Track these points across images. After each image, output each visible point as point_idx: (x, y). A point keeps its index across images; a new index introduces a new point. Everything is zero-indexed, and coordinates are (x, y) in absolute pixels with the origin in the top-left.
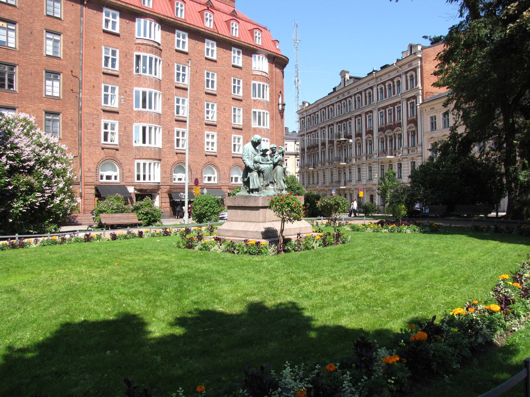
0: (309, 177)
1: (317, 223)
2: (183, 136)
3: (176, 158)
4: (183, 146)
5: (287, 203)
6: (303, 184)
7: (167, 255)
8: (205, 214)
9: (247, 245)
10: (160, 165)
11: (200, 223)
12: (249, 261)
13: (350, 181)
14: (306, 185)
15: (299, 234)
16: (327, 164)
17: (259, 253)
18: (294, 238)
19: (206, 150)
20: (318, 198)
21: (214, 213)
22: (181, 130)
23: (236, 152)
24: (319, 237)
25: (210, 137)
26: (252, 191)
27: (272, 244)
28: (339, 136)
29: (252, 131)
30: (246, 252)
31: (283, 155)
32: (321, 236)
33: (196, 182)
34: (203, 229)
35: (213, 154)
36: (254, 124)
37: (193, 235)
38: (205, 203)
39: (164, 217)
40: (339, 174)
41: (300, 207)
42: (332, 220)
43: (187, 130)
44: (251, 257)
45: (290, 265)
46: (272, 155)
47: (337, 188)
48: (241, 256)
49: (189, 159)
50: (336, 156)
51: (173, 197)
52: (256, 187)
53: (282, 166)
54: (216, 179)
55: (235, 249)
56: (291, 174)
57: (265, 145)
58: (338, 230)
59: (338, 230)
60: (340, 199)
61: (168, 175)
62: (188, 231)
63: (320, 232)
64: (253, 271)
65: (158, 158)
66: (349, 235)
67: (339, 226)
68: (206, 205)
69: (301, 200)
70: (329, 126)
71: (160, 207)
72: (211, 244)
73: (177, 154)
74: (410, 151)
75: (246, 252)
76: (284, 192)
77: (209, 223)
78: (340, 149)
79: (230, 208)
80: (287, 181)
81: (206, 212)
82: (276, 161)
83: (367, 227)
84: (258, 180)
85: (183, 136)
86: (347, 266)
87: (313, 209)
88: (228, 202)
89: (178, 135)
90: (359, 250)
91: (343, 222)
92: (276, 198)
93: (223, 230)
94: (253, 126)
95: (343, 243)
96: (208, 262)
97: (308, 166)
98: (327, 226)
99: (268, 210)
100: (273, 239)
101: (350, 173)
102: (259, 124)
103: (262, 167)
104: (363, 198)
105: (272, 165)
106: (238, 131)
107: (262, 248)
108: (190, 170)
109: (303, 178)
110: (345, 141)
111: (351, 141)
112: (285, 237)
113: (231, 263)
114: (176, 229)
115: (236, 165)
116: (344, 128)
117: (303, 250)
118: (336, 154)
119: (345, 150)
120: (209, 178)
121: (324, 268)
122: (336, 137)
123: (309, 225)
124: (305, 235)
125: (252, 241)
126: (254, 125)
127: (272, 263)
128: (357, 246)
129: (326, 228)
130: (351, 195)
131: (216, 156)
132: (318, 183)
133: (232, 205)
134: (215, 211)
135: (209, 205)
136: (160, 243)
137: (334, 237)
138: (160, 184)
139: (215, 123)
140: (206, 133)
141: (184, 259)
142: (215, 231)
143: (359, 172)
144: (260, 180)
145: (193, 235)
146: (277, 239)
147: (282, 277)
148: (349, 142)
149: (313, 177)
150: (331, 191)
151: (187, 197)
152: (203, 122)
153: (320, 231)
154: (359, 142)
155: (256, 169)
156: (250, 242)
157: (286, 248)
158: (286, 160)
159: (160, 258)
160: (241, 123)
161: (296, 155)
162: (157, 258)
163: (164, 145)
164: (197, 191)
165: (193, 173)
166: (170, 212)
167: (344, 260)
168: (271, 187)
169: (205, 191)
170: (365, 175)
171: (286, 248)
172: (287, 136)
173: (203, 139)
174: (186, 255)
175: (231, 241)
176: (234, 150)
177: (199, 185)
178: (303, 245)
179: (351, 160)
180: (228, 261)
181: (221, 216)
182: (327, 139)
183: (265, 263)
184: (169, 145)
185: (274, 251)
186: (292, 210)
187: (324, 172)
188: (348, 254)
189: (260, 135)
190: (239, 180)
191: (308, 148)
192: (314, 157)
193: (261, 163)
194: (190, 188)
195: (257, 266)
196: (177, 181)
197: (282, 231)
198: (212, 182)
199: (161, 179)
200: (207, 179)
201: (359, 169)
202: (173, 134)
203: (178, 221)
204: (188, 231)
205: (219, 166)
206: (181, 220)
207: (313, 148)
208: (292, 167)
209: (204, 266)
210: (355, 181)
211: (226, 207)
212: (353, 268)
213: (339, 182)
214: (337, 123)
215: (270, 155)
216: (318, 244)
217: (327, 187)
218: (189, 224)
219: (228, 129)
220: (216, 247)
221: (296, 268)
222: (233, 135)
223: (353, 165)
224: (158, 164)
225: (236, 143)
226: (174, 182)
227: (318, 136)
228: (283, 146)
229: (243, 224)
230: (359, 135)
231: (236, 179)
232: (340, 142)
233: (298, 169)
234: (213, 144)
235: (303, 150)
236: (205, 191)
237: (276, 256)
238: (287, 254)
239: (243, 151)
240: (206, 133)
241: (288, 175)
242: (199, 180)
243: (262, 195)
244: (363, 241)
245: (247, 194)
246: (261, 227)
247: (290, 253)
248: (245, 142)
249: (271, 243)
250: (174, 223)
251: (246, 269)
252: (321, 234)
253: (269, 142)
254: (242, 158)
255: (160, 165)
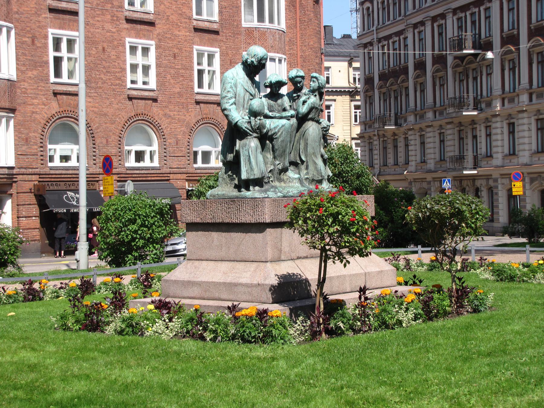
0: (385, 148)
1: (408, 261)
2: (70, 49)
3: (54, 107)
4: (71, 74)
5: (331, 215)
6: (372, 166)
7: (33, 349)
8: (129, 242)
9: (236, 318)
10: (12, 123)
11: (119, 265)
12: (242, 358)
13: (489, 156)
14: (377, 166)
15: (363, 290)
16: (430, 115)
17: (267, 337)
18: (351, 299)
19: (129, 85)
20: (409, 198)
21: (152, 241)
22: (65, 34)
23: (205, 89)
24: (413, 297)
25: (139, 52)
26: (246, 184)
27: (297, 316)
28: (460, 44)
29: (243, 38)
30: (233, 338)
31: (321, 95)
32: (418, 295)
33: (108, 165)
34: (127, 280)
35: (146, 94)
36: (249, 17)
37: (101, 296)
38: (129, 215)
39: (27, 254)
40: (461, 139)
41: (365, 222)
42: (444, 253)
43: (78, 35)
44: (245, 348)
45: (343, 368)
46: (294, 96)
47: (455, 174)
48: (222, 345)
49: (87, 108)
50: (451, 95)
51: (47, 202)
52: (256, 174)
53: (318, 122)
54: (156, 158)
55: (205, 329)
56: (340, 142)
57: (276, 71)
58: (460, 279)
59: (460, 279)
60: (465, 203)
61: (35, 149)
62: (87, 287)
63: (414, 284)
64: (252, 383)
65: (7, 105)
66: (490, 291)
67: (465, 267)
68: (133, 221)
69: (367, 205)
70: (434, 19)
71: (17, 229)
72: (147, 319)
73: (55, 94)
74: (534, 97)
75: (233, 338)
76: (326, 186)
77: (139, 265)
78: (462, 76)
79: (192, 227)
80: (331, 159)
81: (133, 239)
82: (304, 109)
83: (534, 272)
84: (260, 158)
85: (70, 49)
86: (486, 369)
87: (396, 231)
88: (187, 212)
89: (57, 48)
90: (517, 328)
91: (473, 258)
92: (305, 203)
93: (176, 282)
94: (244, 24)
95: (476, 310)
96: (139, 365)
97: (383, 121)
98: (431, 268)
99: (286, 232)
100: (298, 304)
101: (489, 135)
102: (261, 18)
103: (269, 124)
104: (522, 198)
105: (294, 121)
106: (207, 36)
107: (272, 326)
108: (91, 134)
109: (371, 150)
110: (475, 55)
111: (490, 55)
112: (331, 298)
113: (196, 365)
114: (58, 283)
115: (206, 122)
116: (473, 23)
117: (376, 329)
118: (451, 89)
119: (475, 79)
120: (140, 156)
121: (430, 375)
122: (453, 48)
123: (388, 267)
124: (377, 292)
125: (249, 309)
126: (249, 20)
127: (297, 363)
128: (513, 319)
129: (430, 274)
130: (491, 191)
131: (155, 100)
132: (407, 163)
133: (198, 220)
134: (156, 236)
135: (139, 221)
136: (16, 319)
137: (451, 297)
138: (15, 171)
139: (151, 17)
140: (129, 41)
141: (78, 358)
142: (157, 285)
143: (512, 132)
144: (265, 158)
145: (101, 296)
146: (308, 302)
147: (323, 397)
148: (484, 59)
149: (396, 147)
150: (440, 181)
151: (83, 202)
152: (119, 15)
153: (415, 281)
154: (509, 57)
155: (254, 131)
156: (243, 312)
157: (332, 325)
158: (328, 107)
159: (16, 359)
160: (216, 17)
161: (352, 93)
162: (8, 358)
163: (23, 72)
164: (108, 186)
165: (98, 141)
166: (41, 240)
167: (480, 354)
168: (292, 174)
169: (129, 187)
170: (526, 140)
171: (332, 325)
172: (333, 46)
173: (121, 57)
174: (84, 349)
175: (196, 310)
176: (200, 85)
177: (114, 171)
178: (375, 316)
179: (489, 104)
180: (188, 359)
181: (169, 248)
182: (429, 53)
183: (282, 363)
184: (35, 73)
185: (302, 334)
186: (345, 230)
187: (422, 136)
188: (489, 340)
189: (262, 45)
190: (213, 157)
191: (383, 77)
192: (396, 98)
193: (267, 117)
194: (92, 180)
195: (261, 370)
196: (57, 163)
197: (321, 282)
198: (146, 163)
199: (17, 159)
200: (133, 156)
201: (512, 127)
202: (46, 46)
203: (62, 263)
204: (87, 287)
205: (164, 123)
206: (69, 260)
207: (394, 75)
208: (343, 123)
209: (129, 375)
210: (500, 156)
211: (182, 226)
212: (504, 375)
213: (461, 158)
214: (455, 11)
215: (289, 95)
216: (411, 315)
217: (430, 171)
218: (89, 270)
219: (184, 33)
220: (159, 325)
221: (359, 375)
222: (196, 47)
223: (495, 116)
224: (8, 122)
225: (205, 66)
226: (50, 164)
227: (406, 46)
228: (320, 73)
229: (224, 266)
230: (511, 39)
231: (206, 156)
232: (462, 58)
233: (357, 130)
234: (146, 69)
235: (368, 81)
236: (129, 187)
237: (307, 346)
238: (335, 340)
239: (223, 88)
240: (129, 41)
241: (334, 143)
242: (115, 160)
243: (271, 194)
244: (527, 307)
245: (235, 193)
246: (271, 274)
247: (343, 338)
248: (226, 66)
249: (294, 313)
250: (51, 267)
251: (235, 379)
252: (418, 290)
253: (284, 64)
254: (219, 104)
255: (12, 123)
